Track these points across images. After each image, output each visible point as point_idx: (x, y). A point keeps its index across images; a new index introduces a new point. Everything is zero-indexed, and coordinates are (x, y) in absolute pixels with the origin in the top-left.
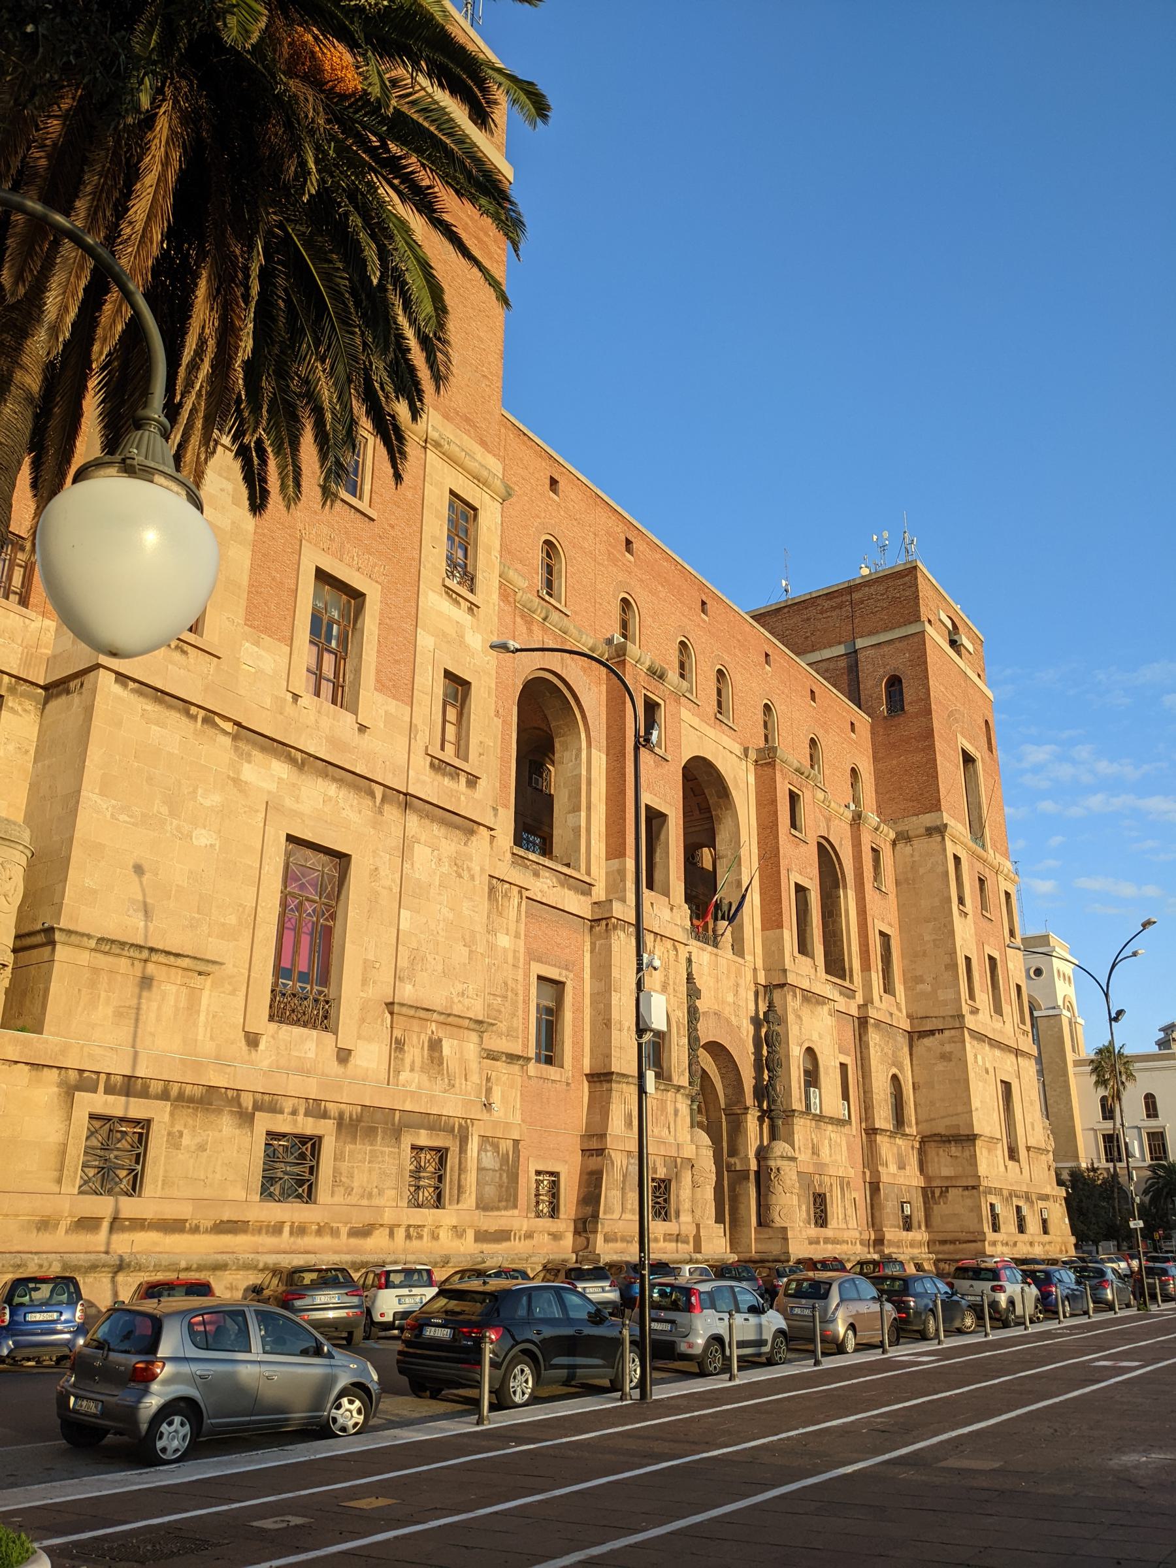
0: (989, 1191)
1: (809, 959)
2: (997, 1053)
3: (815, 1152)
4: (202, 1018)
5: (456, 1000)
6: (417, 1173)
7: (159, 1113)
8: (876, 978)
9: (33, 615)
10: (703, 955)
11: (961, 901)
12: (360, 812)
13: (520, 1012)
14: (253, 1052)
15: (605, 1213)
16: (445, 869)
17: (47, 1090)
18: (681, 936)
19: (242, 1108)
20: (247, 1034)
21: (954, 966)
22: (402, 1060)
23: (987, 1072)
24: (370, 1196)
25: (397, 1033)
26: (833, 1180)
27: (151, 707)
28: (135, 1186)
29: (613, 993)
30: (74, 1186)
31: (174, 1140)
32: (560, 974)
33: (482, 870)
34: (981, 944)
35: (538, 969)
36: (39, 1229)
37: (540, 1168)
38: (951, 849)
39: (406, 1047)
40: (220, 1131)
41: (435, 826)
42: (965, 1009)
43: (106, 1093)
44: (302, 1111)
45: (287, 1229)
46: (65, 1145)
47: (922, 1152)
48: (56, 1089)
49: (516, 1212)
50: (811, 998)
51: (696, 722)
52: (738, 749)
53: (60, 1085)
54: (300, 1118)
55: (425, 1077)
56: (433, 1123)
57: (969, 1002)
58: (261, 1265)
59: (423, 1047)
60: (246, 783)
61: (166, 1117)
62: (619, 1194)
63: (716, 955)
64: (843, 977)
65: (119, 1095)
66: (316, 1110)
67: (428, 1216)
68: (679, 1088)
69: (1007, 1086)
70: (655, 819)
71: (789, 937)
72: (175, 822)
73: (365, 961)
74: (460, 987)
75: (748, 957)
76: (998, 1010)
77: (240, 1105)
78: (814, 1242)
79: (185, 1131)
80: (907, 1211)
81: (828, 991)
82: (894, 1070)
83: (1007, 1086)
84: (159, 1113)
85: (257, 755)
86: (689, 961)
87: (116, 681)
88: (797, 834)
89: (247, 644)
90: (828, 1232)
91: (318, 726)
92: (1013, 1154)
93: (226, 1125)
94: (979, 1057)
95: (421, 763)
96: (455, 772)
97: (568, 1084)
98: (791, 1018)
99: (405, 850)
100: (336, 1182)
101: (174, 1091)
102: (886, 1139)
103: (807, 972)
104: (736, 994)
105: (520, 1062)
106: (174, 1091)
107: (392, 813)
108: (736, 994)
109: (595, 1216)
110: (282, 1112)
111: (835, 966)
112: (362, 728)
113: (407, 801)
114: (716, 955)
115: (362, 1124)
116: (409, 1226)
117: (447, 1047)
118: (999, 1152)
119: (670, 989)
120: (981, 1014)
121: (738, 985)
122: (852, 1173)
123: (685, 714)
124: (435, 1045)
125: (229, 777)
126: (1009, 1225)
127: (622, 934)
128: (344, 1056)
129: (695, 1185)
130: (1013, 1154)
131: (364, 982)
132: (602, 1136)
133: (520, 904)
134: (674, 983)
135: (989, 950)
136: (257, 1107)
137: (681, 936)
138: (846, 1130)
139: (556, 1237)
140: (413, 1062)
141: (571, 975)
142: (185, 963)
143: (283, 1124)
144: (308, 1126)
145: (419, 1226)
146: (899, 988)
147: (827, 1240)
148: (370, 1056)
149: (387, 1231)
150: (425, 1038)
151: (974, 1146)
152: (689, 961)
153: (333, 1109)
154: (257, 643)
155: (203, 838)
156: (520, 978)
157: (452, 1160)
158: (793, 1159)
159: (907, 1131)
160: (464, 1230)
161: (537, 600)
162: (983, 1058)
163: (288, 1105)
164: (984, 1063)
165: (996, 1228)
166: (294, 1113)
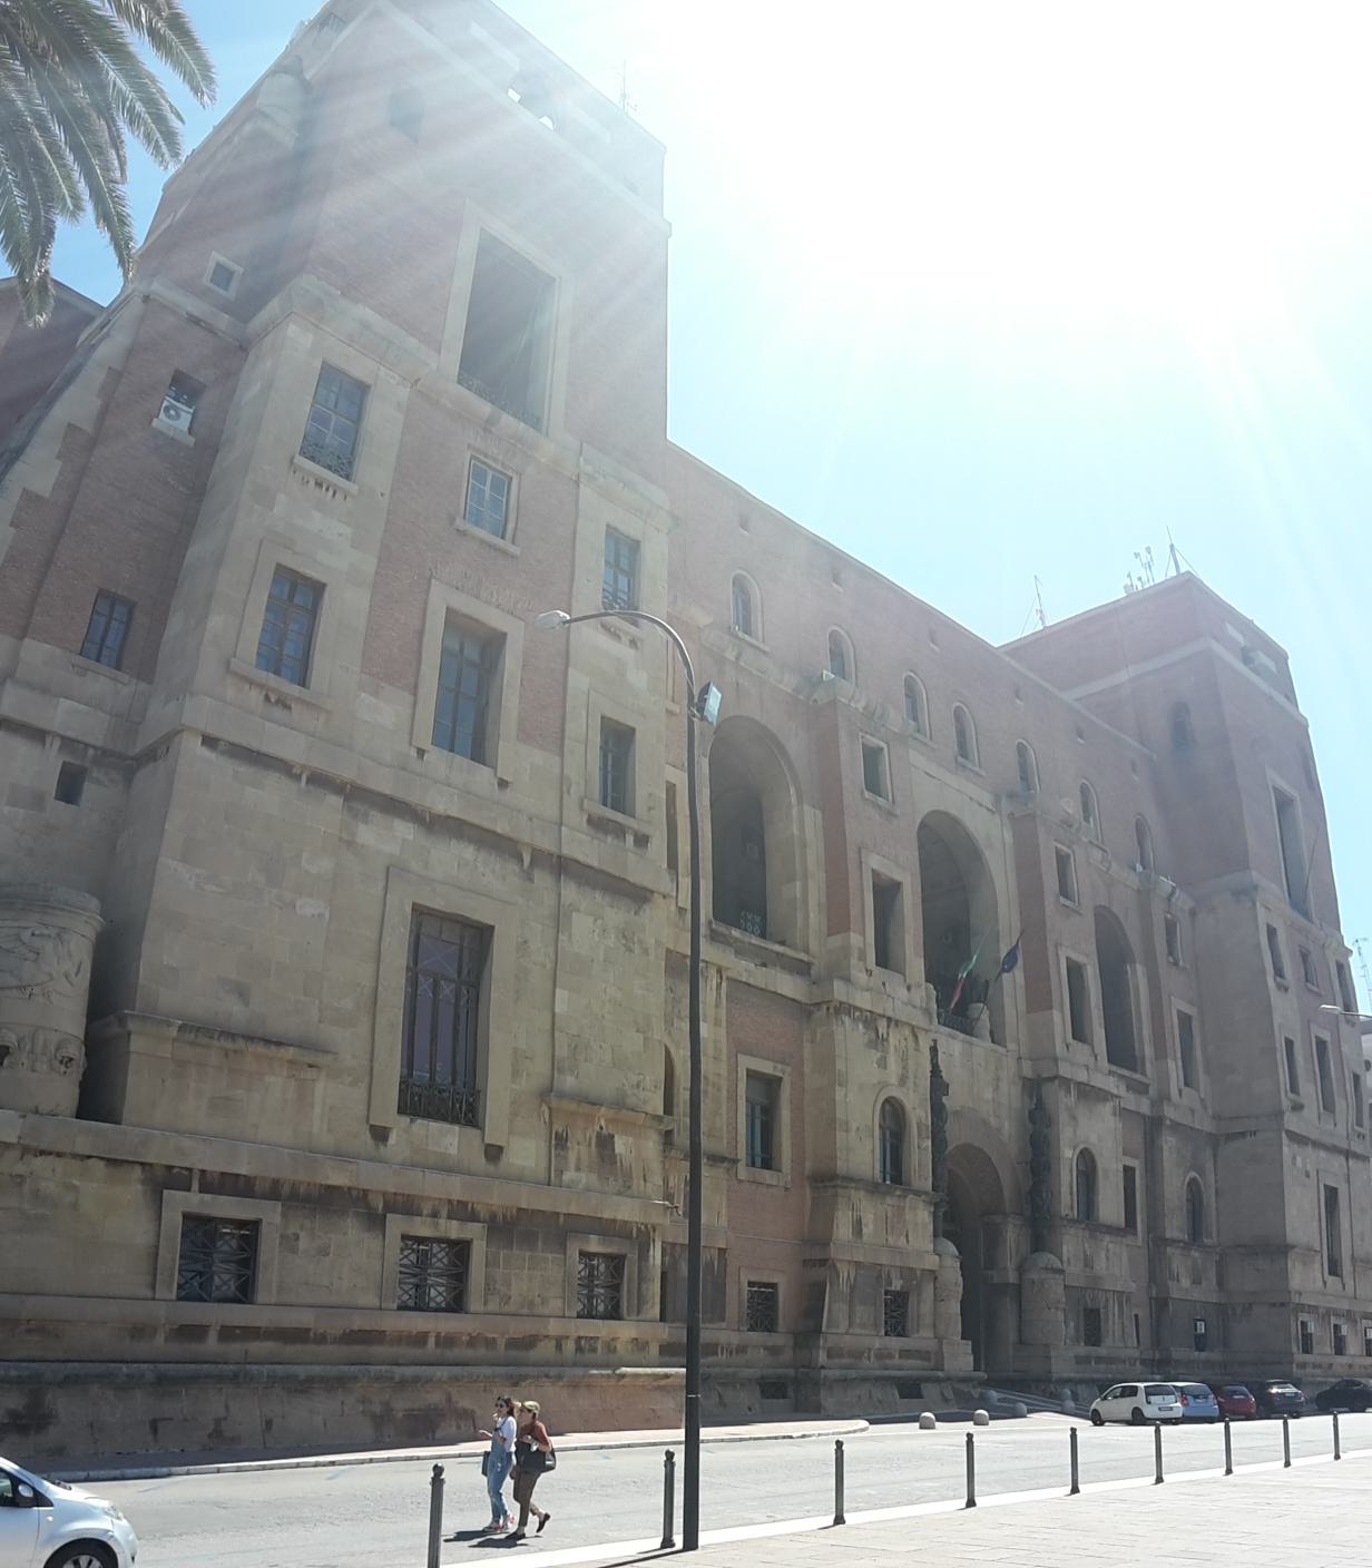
0: (1301, 1308)
1: (1086, 1047)
2: (1323, 1154)
3: (1088, 1263)
4: (318, 1110)
5: (629, 1092)
6: (589, 1282)
7: (271, 1216)
8: (1174, 1068)
9: (125, 678)
10: (953, 1046)
11: (1279, 972)
12: (504, 878)
13: (724, 1110)
14: (382, 1147)
15: (828, 1327)
16: (611, 941)
17: (132, 1189)
18: (919, 1020)
19: (372, 1211)
20: (373, 1128)
21: (1273, 1050)
22: (566, 1158)
23: (1308, 1176)
24: (531, 1304)
25: (558, 1127)
26: (1110, 1295)
27: (245, 770)
28: (245, 1292)
29: (837, 1088)
30: (171, 1291)
31: (289, 1243)
32: (775, 1068)
33: (658, 943)
34: (1307, 1024)
35: (747, 1062)
36: (132, 1337)
37: (753, 1279)
38: (1263, 918)
39: (569, 1144)
40: (345, 1234)
41: (598, 895)
42: (1286, 1104)
43: (200, 1192)
44: (444, 1213)
45: (432, 1341)
46: (157, 1247)
47: (1220, 1265)
48: (139, 1187)
49: (724, 1325)
50: (1089, 1094)
51: (933, 769)
52: (987, 799)
53: (143, 1182)
54: (442, 1221)
55: (594, 1178)
56: (606, 1228)
57: (1291, 1095)
58: (397, 1378)
59: (590, 1145)
60: (363, 846)
61: (278, 1219)
62: (845, 1307)
63: (971, 1044)
64: (1134, 1069)
66: (462, 1212)
67: (601, 1329)
68: (918, 1193)
69: (1332, 1193)
70: (886, 893)
71: (1060, 1019)
72: (275, 891)
73: (515, 1050)
74: (634, 1079)
75: (1012, 1046)
76: (1328, 1105)
77: (368, 1206)
78: (1080, 1360)
79: (302, 1234)
80: (1201, 1328)
81: (1112, 1085)
82: (1193, 1174)
83: (1332, 1193)
84: (271, 1216)
85: (375, 815)
86: (934, 1050)
87: (203, 743)
88: (1068, 903)
89: (363, 695)
90: (1102, 1351)
91: (448, 783)
92: (1335, 1269)
93: (351, 1231)
94: (1299, 1159)
95: (575, 818)
96: (620, 831)
97: (786, 1189)
98: (1063, 1118)
99: (560, 920)
100: (489, 1289)
101: (286, 1190)
102: (1178, 1252)
103: (1086, 1063)
104: (997, 1088)
105: (725, 1164)
106: (286, 1190)
107: (542, 879)
108: (997, 1088)
109: (818, 1331)
110: (420, 1215)
111: (1122, 1053)
112: (503, 784)
113: (562, 866)
114: (971, 1044)
115: (512, 1228)
116: (580, 1338)
117: (620, 1145)
118: (1317, 1266)
119: (910, 1083)
120: (1306, 1112)
121: (998, 1079)
122: (1133, 1287)
123: (916, 758)
124: (605, 1142)
125: (341, 839)
126: (1324, 1348)
127: (847, 1020)
128: (494, 1153)
129: (937, 1299)
130: (1335, 1269)
131: (515, 1073)
132: (825, 1243)
133: (719, 986)
134: (915, 1077)
135: (1316, 1031)
136: (391, 1207)
137: (919, 1020)
138: (1129, 1240)
139: (774, 1351)
140: (579, 1159)
141: (789, 1069)
142: (290, 1053)
143: (422, 1228)
144: (454, 1230)
145: (591, 1338)
146: (1202, 1079)
147: (1099, 1359)
148: (526, 1153)
149: (554, 1342)
150: (592, 1134)
151: (1287, 1257)
152: (934, 1050)
153: (483, 1214)
154: (376, 694)
155: (309, 907)
156: (724, 1072)
157: (630, 1269)
158: (1061, 1272)
159: (1206, 1241)
160: (647, 1343)
161: (727, 637)
162: (1304, 1160)
163: (427, 1208)
164: (1304, 1165)
165: (1307, 1349)
166: (435, 1215)
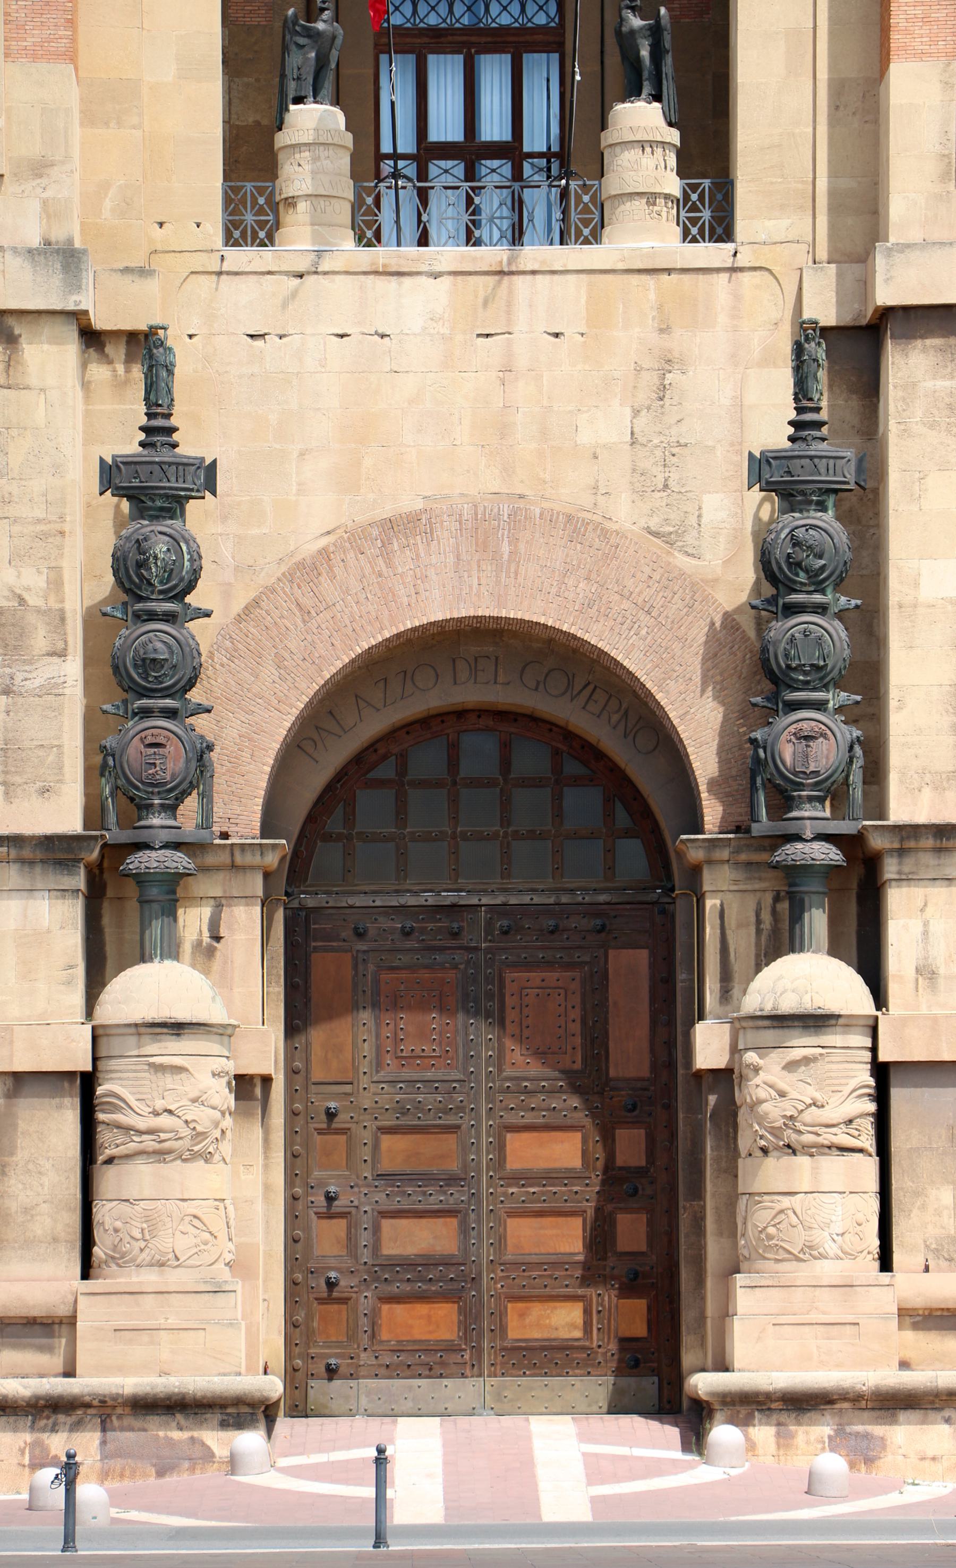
65: (103, 764)
